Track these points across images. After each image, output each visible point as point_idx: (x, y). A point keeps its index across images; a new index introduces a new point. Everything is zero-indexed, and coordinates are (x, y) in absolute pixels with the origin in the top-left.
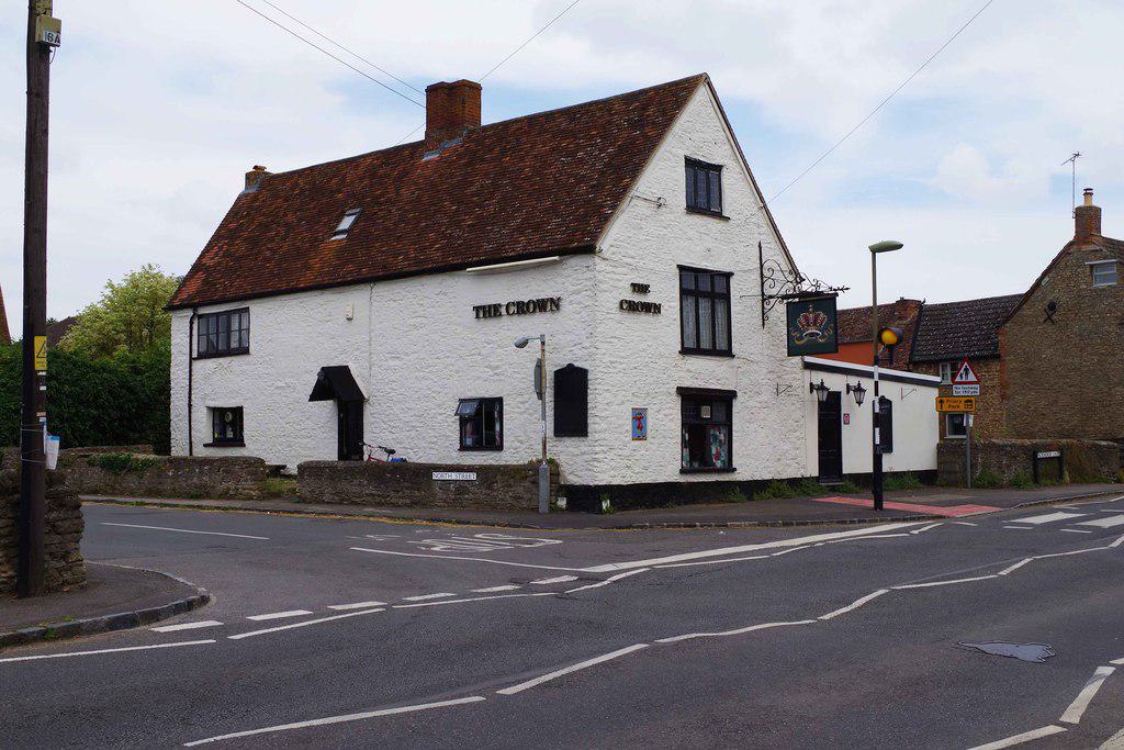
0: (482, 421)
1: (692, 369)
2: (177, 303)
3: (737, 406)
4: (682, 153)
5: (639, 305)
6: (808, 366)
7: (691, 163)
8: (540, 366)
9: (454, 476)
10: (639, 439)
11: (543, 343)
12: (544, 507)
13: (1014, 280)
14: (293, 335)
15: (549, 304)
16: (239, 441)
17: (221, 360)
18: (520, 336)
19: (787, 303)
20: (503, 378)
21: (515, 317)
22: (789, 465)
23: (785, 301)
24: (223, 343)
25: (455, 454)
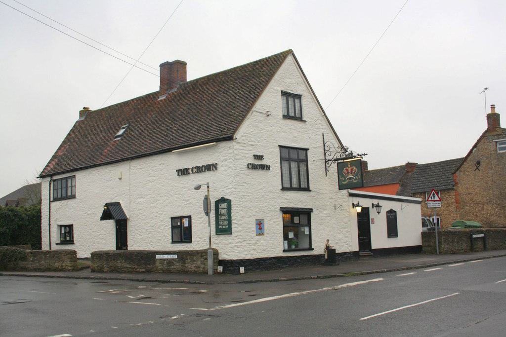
0: (181, 230)
1: (288, 198)
2: (44, 174)
3: (313, 215)
4: (279, 89)
5: (258, 165)
6: (351, 195)
7: (284, 94)
8: (207, 199)
9: (166, 257)
10: (260, 234)
11: (208, 187)
12: (210, 272)
13: (459, 149)
14: (95, 187)
15: (212, 167)
16: (71, 242)
17: (63, 202)
18: (196, 184)
19: (338, 163)
20: (191, 205)
21: (196, 174)
22: (343, 246)
23: (336, 162)
24: (64, 194)
25: (170, 245)
